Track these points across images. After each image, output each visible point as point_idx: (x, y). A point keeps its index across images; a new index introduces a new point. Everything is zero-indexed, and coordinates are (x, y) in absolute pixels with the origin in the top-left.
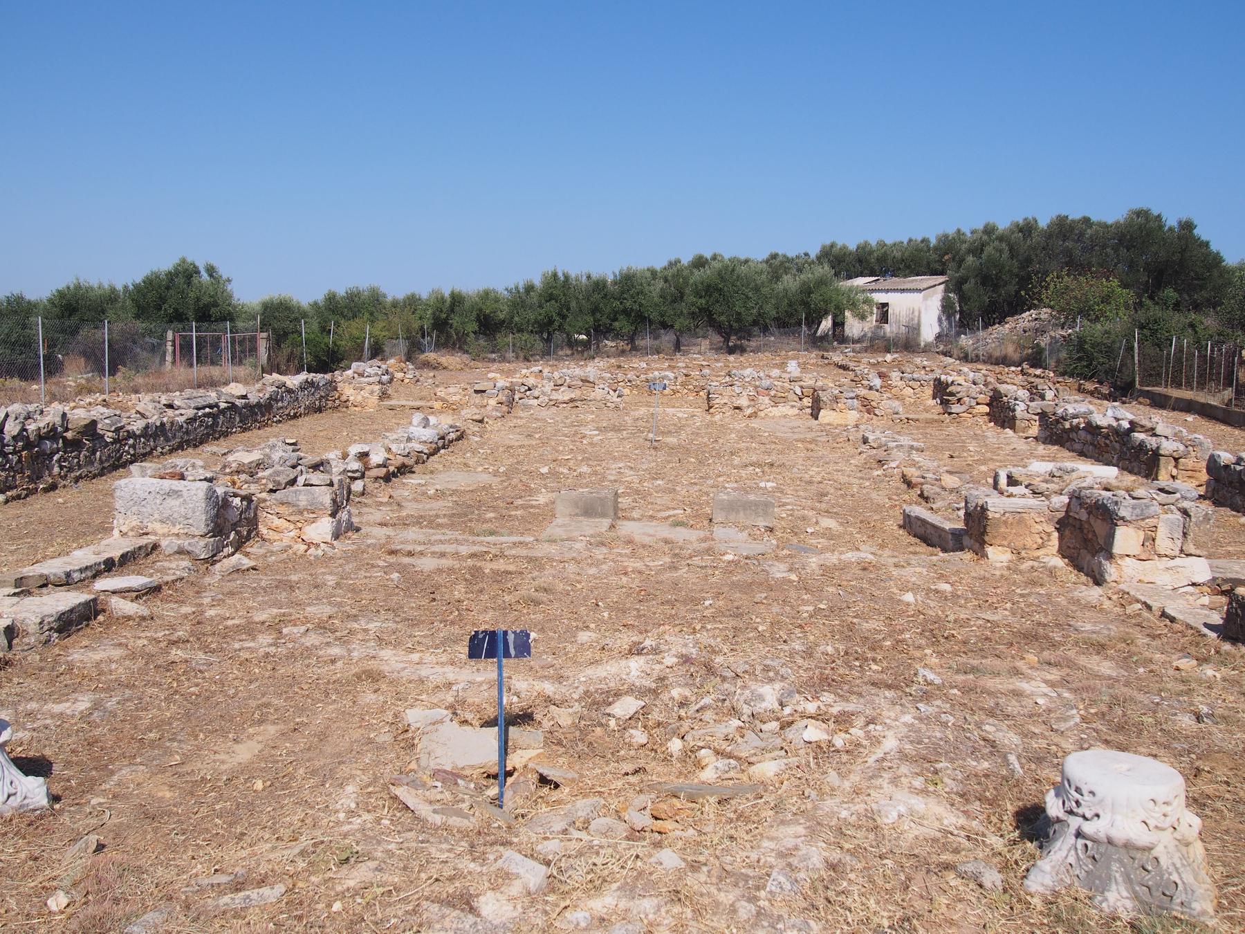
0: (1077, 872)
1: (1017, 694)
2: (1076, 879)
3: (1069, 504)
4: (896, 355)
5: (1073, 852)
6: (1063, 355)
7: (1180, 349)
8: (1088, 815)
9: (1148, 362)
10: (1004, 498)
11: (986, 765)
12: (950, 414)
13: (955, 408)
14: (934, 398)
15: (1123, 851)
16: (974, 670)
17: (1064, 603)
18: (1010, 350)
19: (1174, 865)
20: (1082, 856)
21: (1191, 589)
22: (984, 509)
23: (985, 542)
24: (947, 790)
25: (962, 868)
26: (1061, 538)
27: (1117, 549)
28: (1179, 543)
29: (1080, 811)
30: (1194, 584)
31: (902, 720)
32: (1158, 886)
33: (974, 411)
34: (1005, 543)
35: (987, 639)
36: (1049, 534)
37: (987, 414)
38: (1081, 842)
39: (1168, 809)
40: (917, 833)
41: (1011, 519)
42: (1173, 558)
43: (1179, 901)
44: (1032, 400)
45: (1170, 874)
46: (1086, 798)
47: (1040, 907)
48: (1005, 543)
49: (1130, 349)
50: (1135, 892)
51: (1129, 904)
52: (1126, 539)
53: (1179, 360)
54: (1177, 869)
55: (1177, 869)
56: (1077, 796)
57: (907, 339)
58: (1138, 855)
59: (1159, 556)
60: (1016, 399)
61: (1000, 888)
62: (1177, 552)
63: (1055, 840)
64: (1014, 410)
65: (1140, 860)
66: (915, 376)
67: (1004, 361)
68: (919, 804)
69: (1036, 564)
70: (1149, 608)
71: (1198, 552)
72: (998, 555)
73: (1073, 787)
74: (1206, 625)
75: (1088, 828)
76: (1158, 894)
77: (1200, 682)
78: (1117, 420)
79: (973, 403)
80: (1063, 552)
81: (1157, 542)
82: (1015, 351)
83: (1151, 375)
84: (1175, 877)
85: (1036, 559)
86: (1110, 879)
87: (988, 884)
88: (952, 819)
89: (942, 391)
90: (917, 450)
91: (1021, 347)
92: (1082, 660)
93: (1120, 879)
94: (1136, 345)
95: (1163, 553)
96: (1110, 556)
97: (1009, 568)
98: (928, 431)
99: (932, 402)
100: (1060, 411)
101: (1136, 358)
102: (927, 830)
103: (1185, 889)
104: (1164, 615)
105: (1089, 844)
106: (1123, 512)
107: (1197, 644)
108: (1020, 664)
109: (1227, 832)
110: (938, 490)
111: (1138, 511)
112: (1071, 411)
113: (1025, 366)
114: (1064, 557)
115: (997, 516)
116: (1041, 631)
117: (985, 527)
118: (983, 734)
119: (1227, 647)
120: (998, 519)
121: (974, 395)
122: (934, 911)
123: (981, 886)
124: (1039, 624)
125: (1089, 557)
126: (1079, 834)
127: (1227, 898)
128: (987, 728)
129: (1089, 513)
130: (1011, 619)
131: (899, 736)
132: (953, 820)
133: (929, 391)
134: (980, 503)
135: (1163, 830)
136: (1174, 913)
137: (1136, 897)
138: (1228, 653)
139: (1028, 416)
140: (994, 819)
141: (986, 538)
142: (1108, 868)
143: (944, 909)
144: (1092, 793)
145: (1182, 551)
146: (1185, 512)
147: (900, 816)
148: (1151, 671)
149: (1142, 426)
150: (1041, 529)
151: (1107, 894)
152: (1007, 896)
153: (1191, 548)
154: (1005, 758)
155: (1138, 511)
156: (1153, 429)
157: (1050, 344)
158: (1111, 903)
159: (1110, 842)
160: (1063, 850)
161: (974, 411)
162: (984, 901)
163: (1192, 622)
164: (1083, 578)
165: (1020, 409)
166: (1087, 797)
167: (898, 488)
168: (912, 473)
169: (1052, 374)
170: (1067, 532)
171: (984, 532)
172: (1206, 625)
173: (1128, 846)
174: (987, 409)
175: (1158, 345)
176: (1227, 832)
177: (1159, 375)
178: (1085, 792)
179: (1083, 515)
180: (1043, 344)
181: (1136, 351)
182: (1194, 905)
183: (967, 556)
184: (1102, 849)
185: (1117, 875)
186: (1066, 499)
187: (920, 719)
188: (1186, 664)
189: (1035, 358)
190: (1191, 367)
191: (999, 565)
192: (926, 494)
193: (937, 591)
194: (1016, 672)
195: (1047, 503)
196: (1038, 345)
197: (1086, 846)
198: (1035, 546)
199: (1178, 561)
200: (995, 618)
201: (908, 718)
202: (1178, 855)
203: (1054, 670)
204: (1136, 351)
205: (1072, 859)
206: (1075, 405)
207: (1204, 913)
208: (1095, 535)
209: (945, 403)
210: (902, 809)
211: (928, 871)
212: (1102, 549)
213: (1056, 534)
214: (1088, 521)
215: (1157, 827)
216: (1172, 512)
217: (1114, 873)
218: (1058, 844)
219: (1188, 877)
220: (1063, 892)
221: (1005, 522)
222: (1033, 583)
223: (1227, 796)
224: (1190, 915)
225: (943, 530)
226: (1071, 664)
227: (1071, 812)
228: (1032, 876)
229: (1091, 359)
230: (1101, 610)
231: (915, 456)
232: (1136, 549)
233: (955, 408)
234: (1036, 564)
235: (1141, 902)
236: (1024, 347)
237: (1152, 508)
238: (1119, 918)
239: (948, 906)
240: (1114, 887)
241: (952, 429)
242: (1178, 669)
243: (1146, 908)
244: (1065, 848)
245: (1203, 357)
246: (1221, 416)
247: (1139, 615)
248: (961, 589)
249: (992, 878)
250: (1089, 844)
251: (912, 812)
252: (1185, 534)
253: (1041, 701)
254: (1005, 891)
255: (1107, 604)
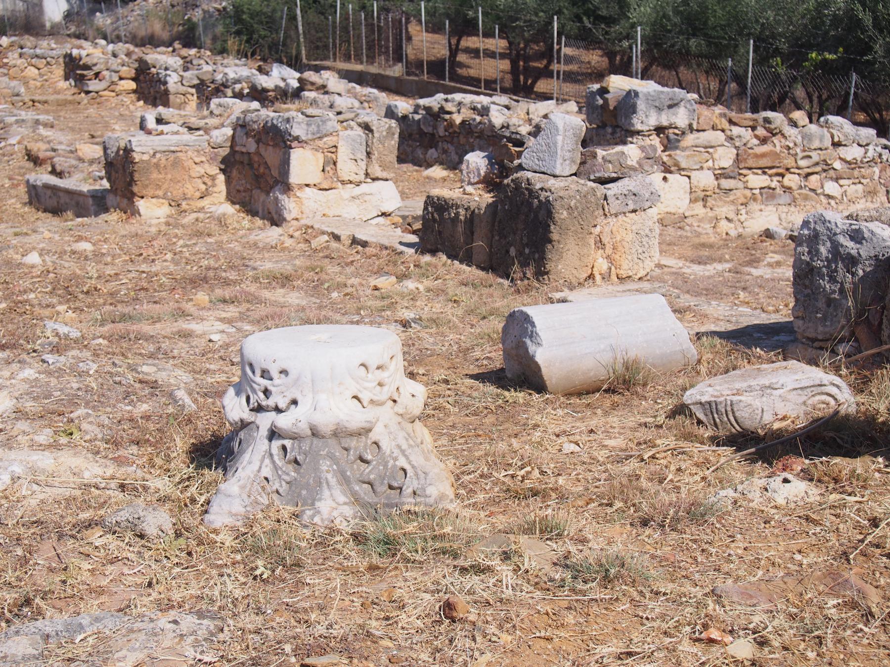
0: (276, 486)
1: (186, 335)
2: (275, 496)
3: (233, 136)
4: (13, 39)
5: (267, 461)
6: (220, 29)
7: (345, 17)
8: (282, 405)
9: (313, 32)
10: (151, 137)
11: (144, 407)
12: (88, 92)
13: (93, 85)
14: (67, 78)
15: (332, 442)
16: (124, 318)
17: (238, 248)
18: (157, 27)
19: (399, 447)
20: (279, 463)
21: (381, 220)
22: (128, 151)
23: (133, 195)
24: (88, 437)
25: (111, 520)
26: (228, 182)
27: (295, 178)
28: (363, 165)
29: (271, 402)
30: (384, 214)
31: (21, 376)
32: (382, 478)
33: (118, 88)
34: (160, 193)
35: (143, 289)
36: (213, 178)
37: (134, 91)
38: (276, 444)
39: (382, 375)
40: (42, 496)
41: (163, 161)
42: (358, 184)
43: (410, 490)
44: (186, 69)
45: (395, 459)
46: (276, 381)
47: (229, 541)
48: (160, 193)
49: (294, 18)
50: (354, 494)
51: (348, 511)
52: (303, 164)
53: (345, 29)
54: (403, 452)
55: (403, 452)
56: (265, 382)
57: (27, 17)
58: (353, 443)
59: (343, 182)
60: (166, 69)
61: (171, 532)
62: (362, 177)
63: (241, 452)
64: (165, 83)
65: (356, 449)
66: (38, 51)
67: (152, 41)
68: (45, 461)
69: (201, 216)
70: (337, 238)
71: (384, 175)
72: (152, 210)
73: (258, 372)
74: (401, 243)
75: (284, 421)
76: (382, 488)
77: (402, 296)
78: (284, 80)
79: (115, 78)
80: (232, 198)
81: (339, 165)
82: (164, 28)
83: (317, 48)
84: (402, 462)
85: (201, 210)
86: (320, 484)
87: (151, 530)
88: (94, 470)
89: (75, 69)
90: (45, 125)
91: (168, 23)
92: (266, 294)
93: (333, 481)
94: (299, 12)
95: (346, 178)
96: (287, 188)
97: (168, 224)
98: (62, 114)
99: (63, 84)
100: (219, 77)
101: (300, 28)
102: (61, 491)
103: (417, 475)
104: (355, 241)
105: (288, 443)
106: (296, 131)
107: (395, 264)
108: (189, 307)
109: (453, 426)
110: (74, 162)
111: (313, 128)
112: (232, 75)
113: (177, 45)
114: (233, 203)
115: (146, 157)
116: (211, 274)
117: (131, 175)
118: (141, 376)
119: (427, 258)
120: (148, 162)
121: (114, 67)
122: (69, 581)
123: (142, 536)
124: (208, 268)
125: (263, 197)
126: (273, 434)
127: (465, 487)
128: (145, 369)
129: (258, 142)
130: (172, 268)
131: (17, 394)
132: (99, 471)
133: (59, 71)
134: (122, 145)
135: (381, 404)
136: (406, 507)
137: (357, 500)
138: (428, 264)
139: (183, 89)
140: (159, 461)
141: (135, 189)
142: (316, 469)
143: (86, 576)
144: (284, 372)
145: (367, 175)
146: (367, 127)
147: (15, 479)
148: (347, 294)
149: (313, 84)
150: (202, 171)
151: (318, 504)
152: (182, 541)
153: (376, 171)
154: (171, 395)
155: (313, 128)
156: (324, 87)
157: (204, 19)
158: (325, 516)
159: (315, 433)
160: (255, 460)
161: (118, 88)
162: (147, 554)
163: (386, 242)
164: (259, 222)
165: (173, 80)
166: (278, 379)
167: (21, 168)
168: (40, 149)
169: (208, 53)
170: (235, 173)
171: (132, 182)
172: (401, 243)
173: (339, 433)
174: (133, 85)
175: (323, 14)
176: (453, 426)
177: (326, 47)
178: (274, 374)
179: (251, 146)
180: (195, 19)
181: (299, 18)
182: (430, 490)
183: (113, 217)
184: (305, 446)
185: (329, 476)
186: (229, 132)
187: (49, 373)
188: (386, 282)
189: (187, 37)
190: (359, 36)
191: (155, 222)
192: (58, 168)
193: (74, 252)
194: (183, 314)
195: (206, 137)
196: (189, 20)
197: (284, 448)
198: (198, 194)
199: (364, 188)
200: (154, 269)
201: (29, 373)
202: (401, 435)
203: (232, 308)
204: (299, 18)
205: (267, 471)
206: (236, 69)
207: (442, 497)
208: (267, 167)
209: (80, 80)
210: (18, 469)
211: (61, 537)
212: (277, 182)
213: (221, 177)
214: (258, 153)
215: (372, 402)
216: (352, 128)
217: (324, 475)
218: (246, 457)
219: (417, 459)
220: (260, 515)
221: (157, 165)
222: (199, 234)
223: (448, 392)
224: (426, 505)
225: (80, 194)
226: (252, 299)
227: (259, 409)
228: (214, 508)
229: (250, 32)
230: (283, 249)
231: (42, 131)
232: (315, 176)
233: (93, 85)
234: (201, 216)
235: (364, 505)
236: (174, 24)
237: (329, 123)
238: (339, 532)
239: (92, 571)
240: (326, 493)
241: (92, 111)
242: (376, 288)
243: (371, 512)
244: (257, 458)
245: (370, 26)
246: (393, 85)
247: (327, 248)
248: (105, 248)
249: (157, 521)
250: (288, 443)
251: (33, 470)
252: (368, 154)
253: (215, 337)
254: (178, 535)
255: (289, 242)
